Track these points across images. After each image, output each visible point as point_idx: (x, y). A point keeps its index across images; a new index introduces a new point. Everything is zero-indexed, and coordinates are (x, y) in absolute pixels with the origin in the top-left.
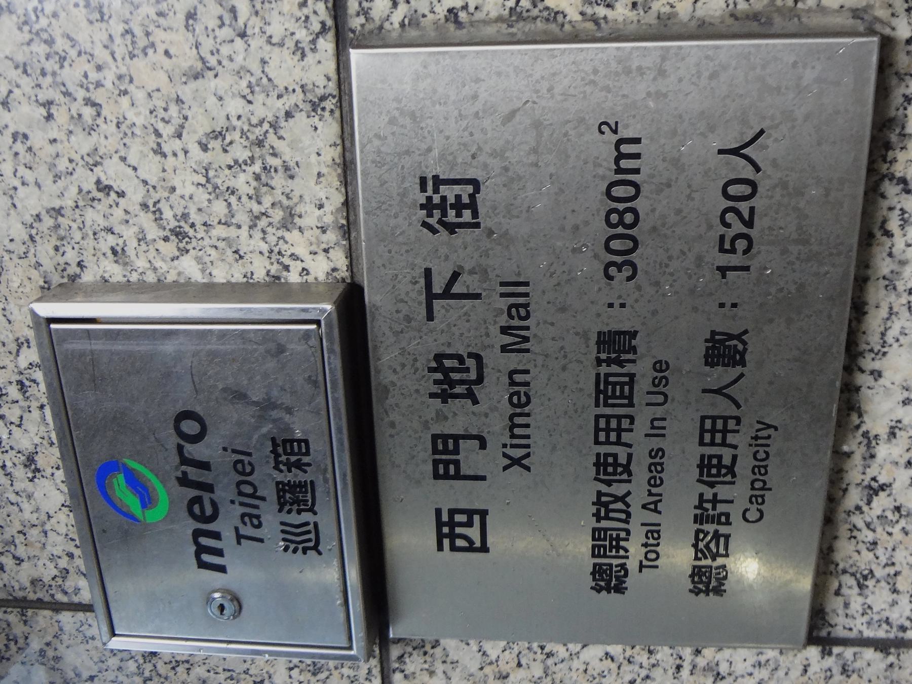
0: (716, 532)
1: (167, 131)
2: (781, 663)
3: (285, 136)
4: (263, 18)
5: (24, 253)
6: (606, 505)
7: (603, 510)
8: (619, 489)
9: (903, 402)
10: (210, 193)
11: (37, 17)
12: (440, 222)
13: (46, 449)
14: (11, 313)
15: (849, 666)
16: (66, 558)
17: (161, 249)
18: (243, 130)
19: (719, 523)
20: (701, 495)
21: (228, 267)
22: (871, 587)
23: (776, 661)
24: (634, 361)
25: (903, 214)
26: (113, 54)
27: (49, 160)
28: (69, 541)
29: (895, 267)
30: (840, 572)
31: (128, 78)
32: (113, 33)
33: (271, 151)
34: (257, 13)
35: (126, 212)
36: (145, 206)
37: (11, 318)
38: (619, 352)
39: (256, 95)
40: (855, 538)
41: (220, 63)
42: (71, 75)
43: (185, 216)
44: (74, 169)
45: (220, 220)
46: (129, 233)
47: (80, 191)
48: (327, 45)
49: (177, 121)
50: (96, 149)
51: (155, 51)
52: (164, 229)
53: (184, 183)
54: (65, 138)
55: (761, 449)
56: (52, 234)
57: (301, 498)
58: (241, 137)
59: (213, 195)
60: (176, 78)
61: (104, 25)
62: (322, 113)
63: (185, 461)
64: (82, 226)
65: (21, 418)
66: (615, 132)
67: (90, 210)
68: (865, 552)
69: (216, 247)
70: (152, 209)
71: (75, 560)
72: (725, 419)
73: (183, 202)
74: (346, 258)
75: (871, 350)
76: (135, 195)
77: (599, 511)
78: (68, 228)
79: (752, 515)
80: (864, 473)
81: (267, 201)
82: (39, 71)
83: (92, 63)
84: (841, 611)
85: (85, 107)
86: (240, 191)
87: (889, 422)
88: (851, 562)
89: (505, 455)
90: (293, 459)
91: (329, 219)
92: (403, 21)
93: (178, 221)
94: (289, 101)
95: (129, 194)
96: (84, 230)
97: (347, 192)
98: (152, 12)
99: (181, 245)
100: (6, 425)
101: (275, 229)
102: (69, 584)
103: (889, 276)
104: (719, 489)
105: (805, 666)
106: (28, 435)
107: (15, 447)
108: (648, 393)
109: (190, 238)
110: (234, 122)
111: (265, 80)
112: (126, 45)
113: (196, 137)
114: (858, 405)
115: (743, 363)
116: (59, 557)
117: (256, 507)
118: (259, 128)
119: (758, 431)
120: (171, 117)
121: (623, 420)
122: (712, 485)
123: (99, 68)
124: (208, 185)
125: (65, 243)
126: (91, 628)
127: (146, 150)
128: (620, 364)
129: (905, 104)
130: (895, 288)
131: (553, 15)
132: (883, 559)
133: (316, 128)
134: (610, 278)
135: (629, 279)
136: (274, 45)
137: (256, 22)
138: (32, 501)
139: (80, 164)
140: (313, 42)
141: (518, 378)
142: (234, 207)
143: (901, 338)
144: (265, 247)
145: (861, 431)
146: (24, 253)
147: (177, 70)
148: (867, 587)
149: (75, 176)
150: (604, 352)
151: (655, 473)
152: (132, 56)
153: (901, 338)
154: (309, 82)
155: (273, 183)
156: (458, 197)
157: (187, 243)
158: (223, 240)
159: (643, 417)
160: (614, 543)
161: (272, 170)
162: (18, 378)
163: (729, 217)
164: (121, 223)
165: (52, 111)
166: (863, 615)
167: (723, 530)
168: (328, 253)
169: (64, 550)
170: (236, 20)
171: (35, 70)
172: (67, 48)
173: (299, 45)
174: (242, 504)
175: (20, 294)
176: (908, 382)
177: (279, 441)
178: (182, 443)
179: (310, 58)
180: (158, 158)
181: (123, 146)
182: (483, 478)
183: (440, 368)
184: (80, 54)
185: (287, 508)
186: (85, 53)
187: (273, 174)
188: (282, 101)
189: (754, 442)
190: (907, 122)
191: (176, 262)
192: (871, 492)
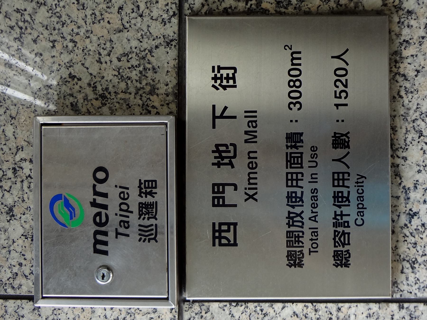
0: (343, 231)
1: (104, 53)
2: (380, 315)
3: (154, 56)
4: (150, 10)
5: (30, 106)
6: (292, 218)
7: (291, 221)
8: (298, 210)
9: (418, 171)
10: (119, 79)
11: (56, 7)
12: (220, 85)
13: (20, 204)
14: (17, 134)
15: (413, 315)
16: (18, 266)
17: (94, 103)
18: (137, 53)
19: (345, 227)
20: (335, 212)
21: (123, 111)
22: (417, 268)
23: (378, 313)
24: (302, 146)
25: (406, 89)
26: (85, 22)
27: (50, 65)
28: (22, 256)
29: (405, 111)
30: (402, 260)
31: (91, 31)
32: (87, 14)
33: (148, 62)
34: (148, 8)
35: (81, 87)
36: (89, 85)
37: (16, 136)
38: (296, 142)
39: (144, 39)
40: (406, 241)
41: (130, 26)
42: (66, 30)
43: (107, 89)
44: (60, 68)
45: (122, 91)
46: (80, 97)
47: (61, 78)
48: (175, 20)
49: (108, 49)
50: (72, 60)
51: (104, 21)
52: (97, 94)
53: (108, 75)
54: (58, 56)
55: (360, 188)
56: (44, 97)
57: (150, 211)
58: (136, 56)
59: (121, 80)
60: (111, 32)
61: (84, 11)
62: (171, 47)
63: (96, 193)
64: (59, 93)
65: (11, 187)
66: (291, 49)
67: (64, 86)
68: (412, 249)
69: (119, 103)
70: (92, 86)
71: (22, 268)
72: (343, 173)
73: (107, 83)
74: (176, 107)
75: (401, 148)
76: (86, 79)
77: (289, 221)
78: (53, 94)
79: (359, 222)
80: (406, 207)
81: (144, 82)
82: (53, 28)
83: (76, 25)
84: (405, 282)
85: (70, 43)
86: (132, 78)
87: (413, 181)
88: (406, 254)
89: (246, 193)
90: (148, 190)
91: (170, 90)
92: (206, 12)
93: (103, 91)
94: (157, 42)
95: (83, 79)
96: (59, 95)
97: (179, 80)
98: (104, 6)
99: (103, 102)
100: (2, 191)
101: (146, 95)
102: (16, 283)
103: (404, 114)
104: (343, 208)
105: (392, 316)
106: (12, 196)
107: (4, 203)
108: (309, 161)
109: (108, 99)
110: (134, 49)
111: (148, 33)
112: (92, 19)
113: (116, 56)
114: (399, 173)
115: (348, 147)
116: (14, 266)
117: (128, 217)
118: (144, 52)
119: (358, 179)
120: (107, 47)
121: (299, 175)
122: (340, 207)
123: (79, 27)
124: (119, 76)
125: (50, 101)
126: (23, 310)
127: (94, 60)
128: (296, 147)
129: (400, 45)
130: (407, 120)
131: (264, 11)
132: (421, 253)
133: (168, 53)
134: (291, 109)
135: (299, 109)
136: (153, 20)
137: (147, 11)
138: (6, 234)
139: (63, 66)
140: (170, 19)
141: (252, 155)
142: (129, 85)
143: (413, 142)
144: (140, 102)
145: (402, 186)
146: (30, 106)
147: (112, 29)
148: (415, 268)
149: (60, 71)
150: (289, 142)
151: (314, 201)
152: (94, 23)
153: (413, 142)
154: (166, 34)
155: (147, 75)
156: (228, 75)
157: (106, 101)
158: (123, 99)
159: (307, 172)
160: (297, 239)
161: (148, 69)
162: (14, 166)
163: (338, 83)
164: (77, 92)
165: (55, 44)
166: (415, 284)
167: (347, 230)
168: (169, 105)
169: (18, 262)
170: (139, 10)
171: (50, 27)
172: (67, 19)
173: (164, 20)
174: (121, 215)
175: (23, 125)
176: (419, 162)
177: (143, 181)
178: (96, 183)
179: (168, 25)
180: (99, 64)
181: (84, 59)
182: (235, 206)
183: (217, 151)
184: (71, 22)
185: (142, 217)
186: (74, 22)
187: (148, 71)
188: (154, 41)
189: (356, 185)
190: (402, 52)
191: (100, 109)
192: (410, 216)
